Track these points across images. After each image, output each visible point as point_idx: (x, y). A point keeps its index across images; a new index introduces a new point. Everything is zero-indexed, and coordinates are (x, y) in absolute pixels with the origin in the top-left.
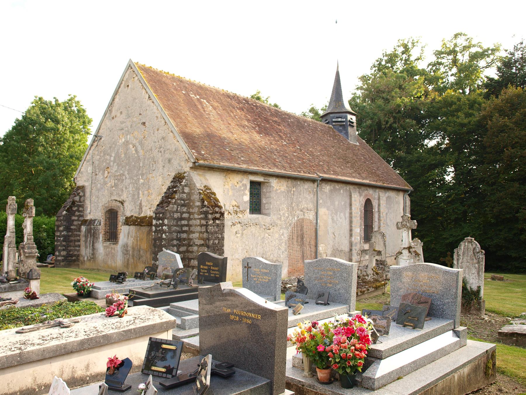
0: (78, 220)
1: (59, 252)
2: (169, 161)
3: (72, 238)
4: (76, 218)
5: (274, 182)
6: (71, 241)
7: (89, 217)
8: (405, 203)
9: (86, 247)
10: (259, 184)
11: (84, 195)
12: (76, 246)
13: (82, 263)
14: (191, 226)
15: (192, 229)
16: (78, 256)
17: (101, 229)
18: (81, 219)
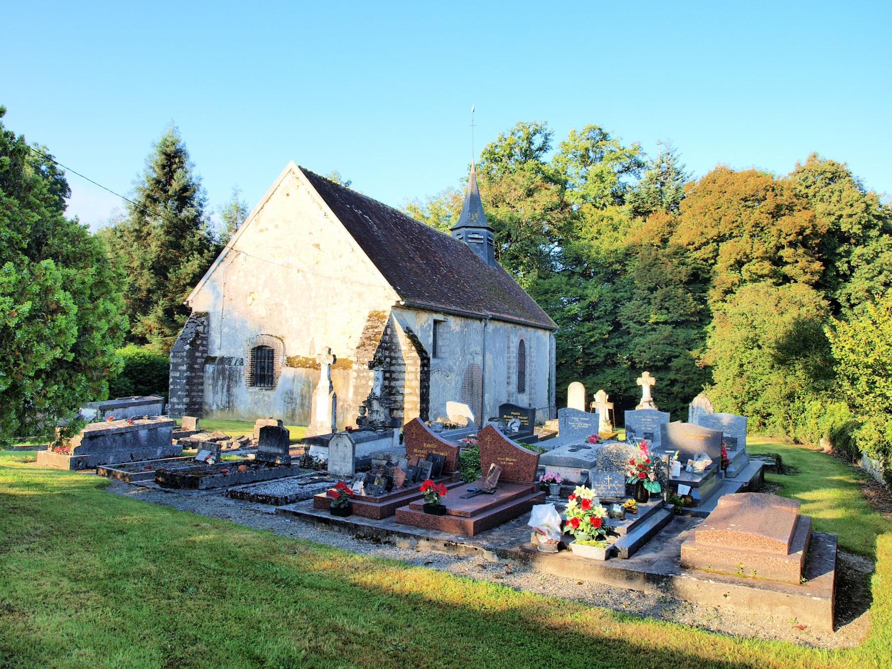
0: (202, 357)
1: (179, 397)
2: (360, 295)
3: (195, 381)
4: (200, 354)
5: (451, 320)
6: (194, 385)
7: (217, 353)
8: (551, 345)
9: (215, 393)
10: (440, 322)
11: (208, 325)
12: (199, 391)
13: (207, 413)
14: (393, 372)
15: (394, 375)
16: (201, 404)
17: (245, 371)
18: (205, 355)
